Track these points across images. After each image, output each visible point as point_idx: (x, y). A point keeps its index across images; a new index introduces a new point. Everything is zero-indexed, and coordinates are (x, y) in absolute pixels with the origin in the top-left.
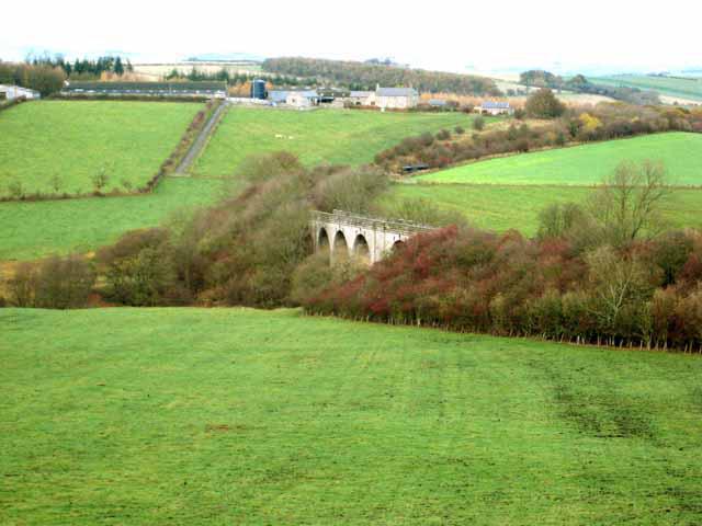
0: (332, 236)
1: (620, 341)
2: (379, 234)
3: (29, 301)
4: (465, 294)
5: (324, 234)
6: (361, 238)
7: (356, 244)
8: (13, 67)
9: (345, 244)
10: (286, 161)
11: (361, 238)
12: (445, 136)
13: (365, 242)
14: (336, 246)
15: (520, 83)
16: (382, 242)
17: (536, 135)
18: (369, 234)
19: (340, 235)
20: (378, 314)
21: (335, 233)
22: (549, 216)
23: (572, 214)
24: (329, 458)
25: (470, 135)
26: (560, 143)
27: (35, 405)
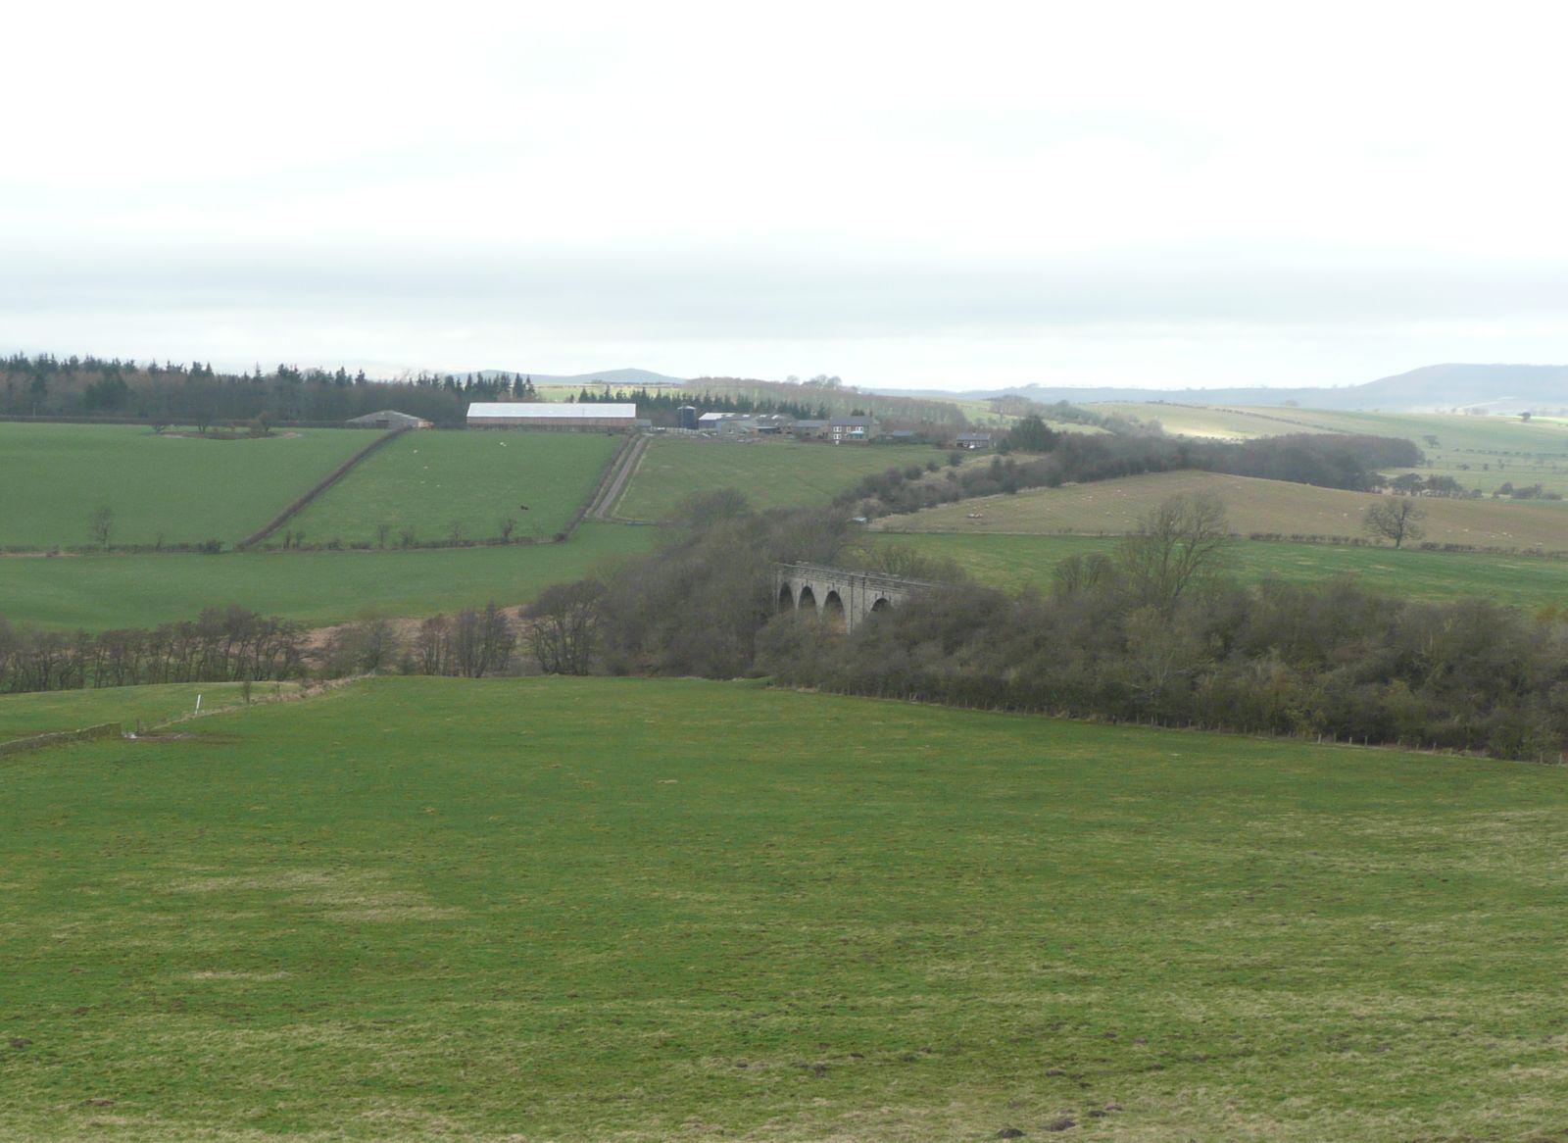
0: (797, 593)
1: (1166, 720)
2: (858, 590)
3: (437, 668)
4: (964, 664)
5: (786, 592)
6: (833, 597)
7: (827, 603)
8: (373, 383)
9: (814, 602)
10: (730, 504)
11: (833, 597)
12: (915, 474)
13: (839, 599)
14: (801, 605)
15: (991, 411)
16: (860, 599)
17: (1023, 471)
18: (844, 591)
19: (807, 592)
20: (865, 686)
21: (801, 590)
22: (1070, 573)
23: (1100, 568)
24: (536, 1018)
25: (945, 474)
26: (1055, 482)
27: (13, 953)
